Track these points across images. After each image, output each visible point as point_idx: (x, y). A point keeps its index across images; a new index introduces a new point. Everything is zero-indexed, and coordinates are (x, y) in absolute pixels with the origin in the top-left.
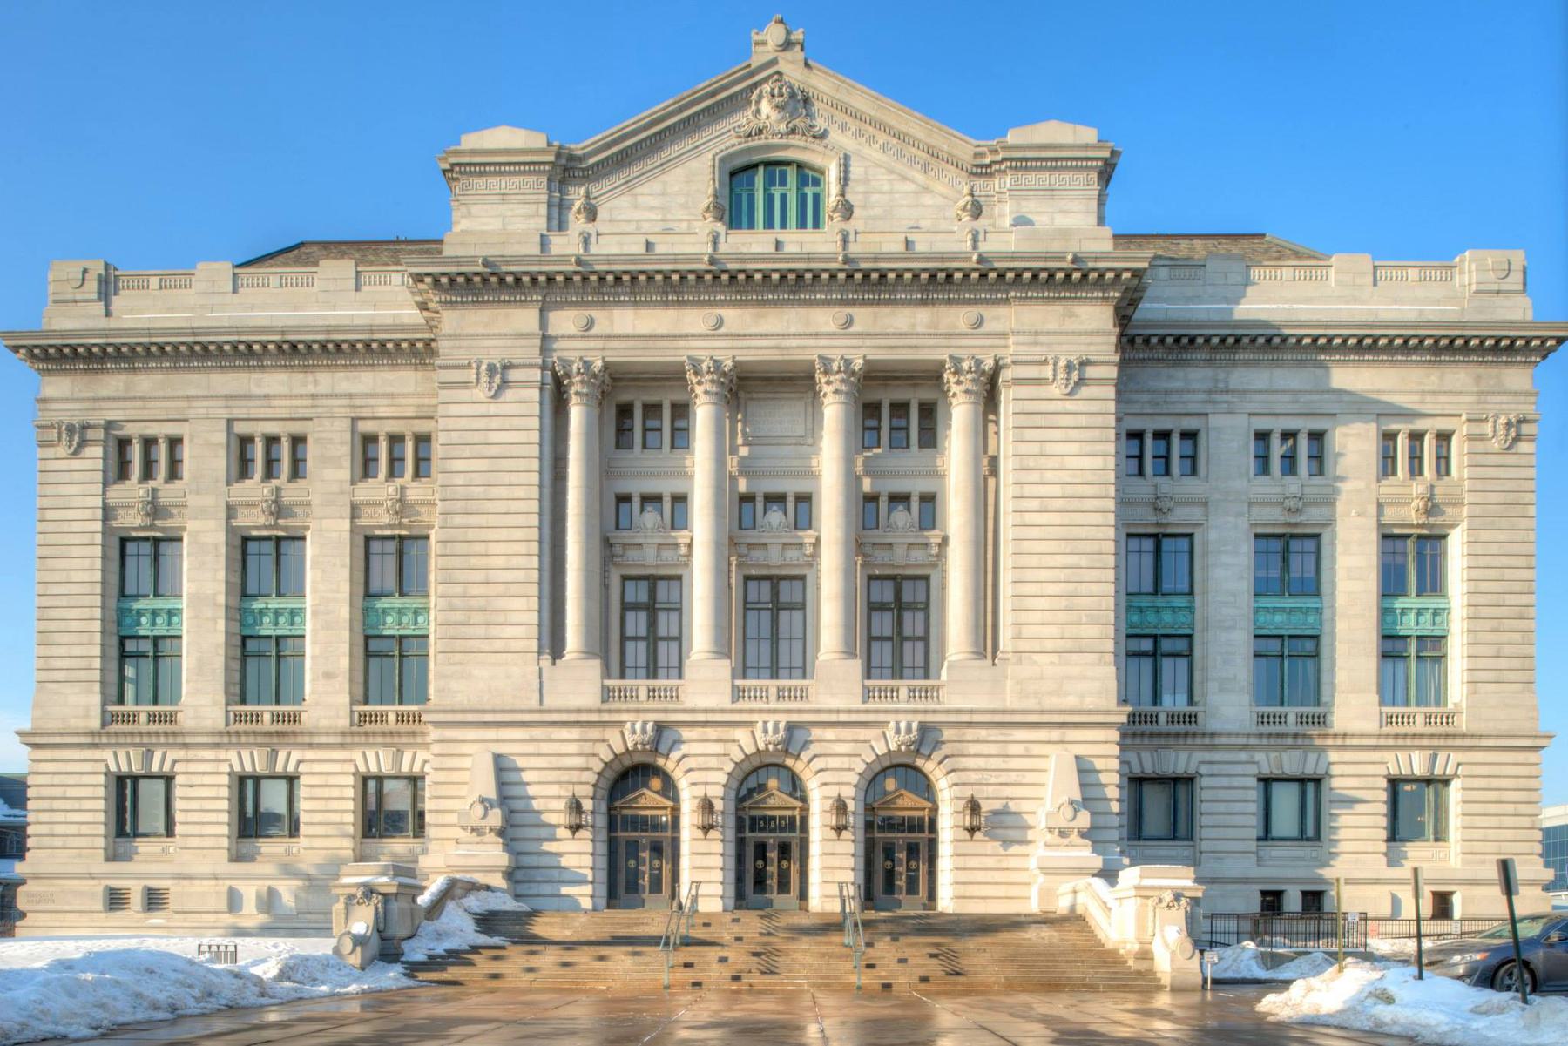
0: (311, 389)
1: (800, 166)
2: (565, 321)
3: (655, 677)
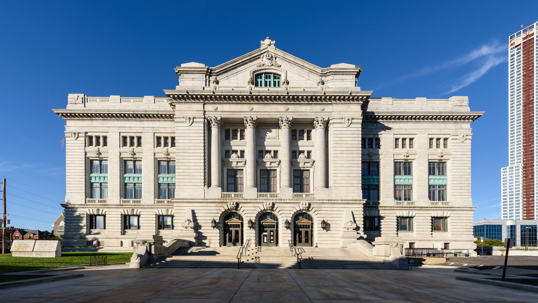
0: (142, 126)
1: (274, 74)
2: (209, 107)
3: (236, 191)
